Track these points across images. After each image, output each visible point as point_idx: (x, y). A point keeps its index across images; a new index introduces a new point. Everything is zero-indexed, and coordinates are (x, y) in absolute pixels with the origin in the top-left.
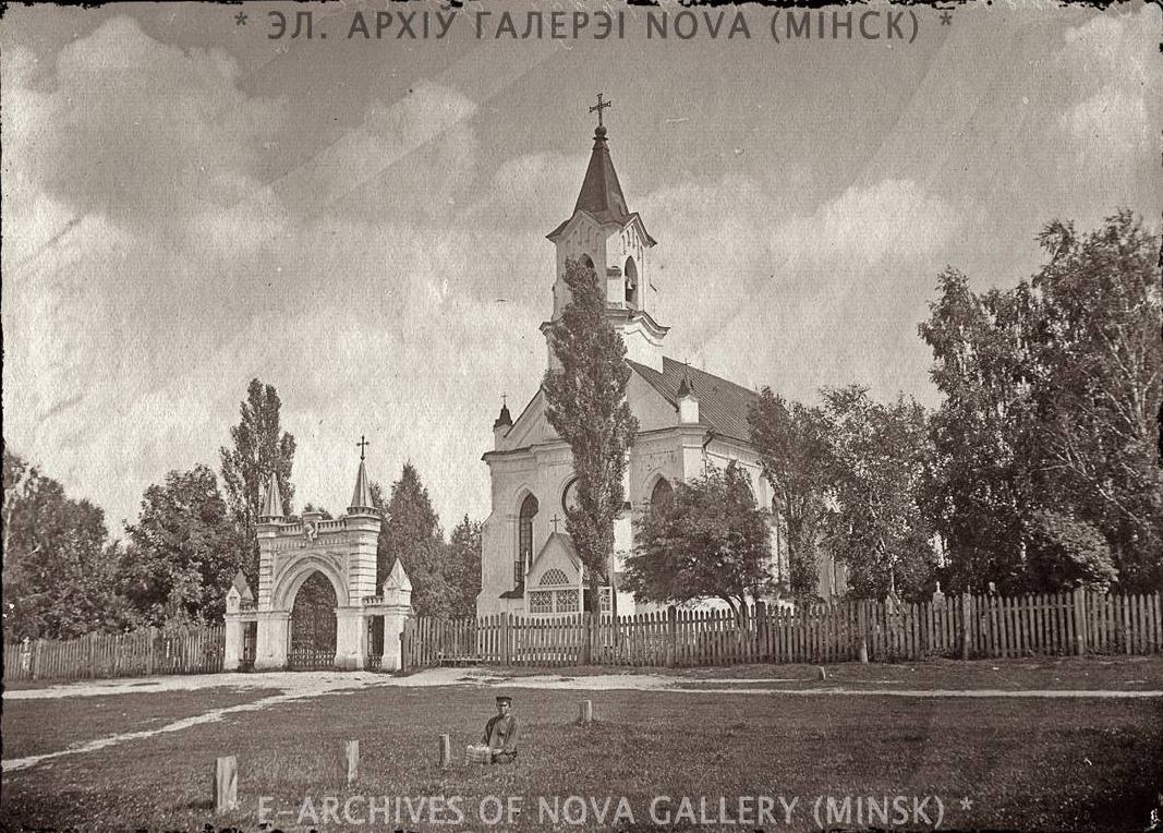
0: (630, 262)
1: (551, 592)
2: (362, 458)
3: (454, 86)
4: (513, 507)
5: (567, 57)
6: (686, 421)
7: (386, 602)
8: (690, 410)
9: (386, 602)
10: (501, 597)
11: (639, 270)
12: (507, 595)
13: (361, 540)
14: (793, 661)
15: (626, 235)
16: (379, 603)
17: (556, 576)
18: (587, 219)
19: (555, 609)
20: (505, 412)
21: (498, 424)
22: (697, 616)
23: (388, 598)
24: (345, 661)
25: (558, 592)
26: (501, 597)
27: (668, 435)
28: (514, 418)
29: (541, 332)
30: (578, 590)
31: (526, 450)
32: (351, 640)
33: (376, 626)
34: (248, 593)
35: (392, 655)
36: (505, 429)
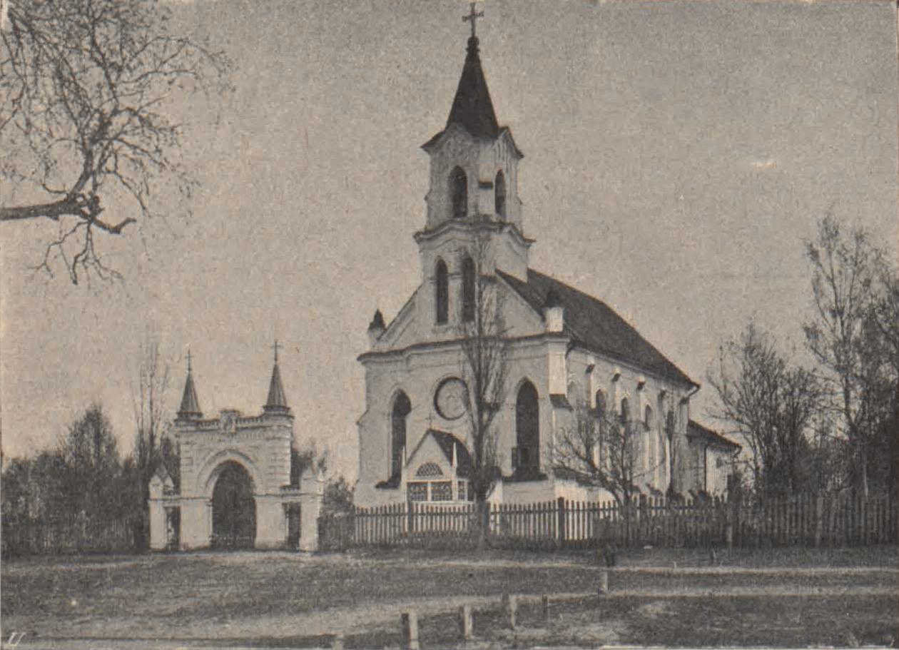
1: (426, 483)
4: (385, 405)
6: (551, 330)
9: (302, 491)
10: (377, 487)
12: (382, 486)
14: (735, 544)
20: (378, 318)
23: (304, 486)
26: (377, 487)
27: (527, 343)
28: (387, 322)
33: (293, 512)
35: (309, 538)
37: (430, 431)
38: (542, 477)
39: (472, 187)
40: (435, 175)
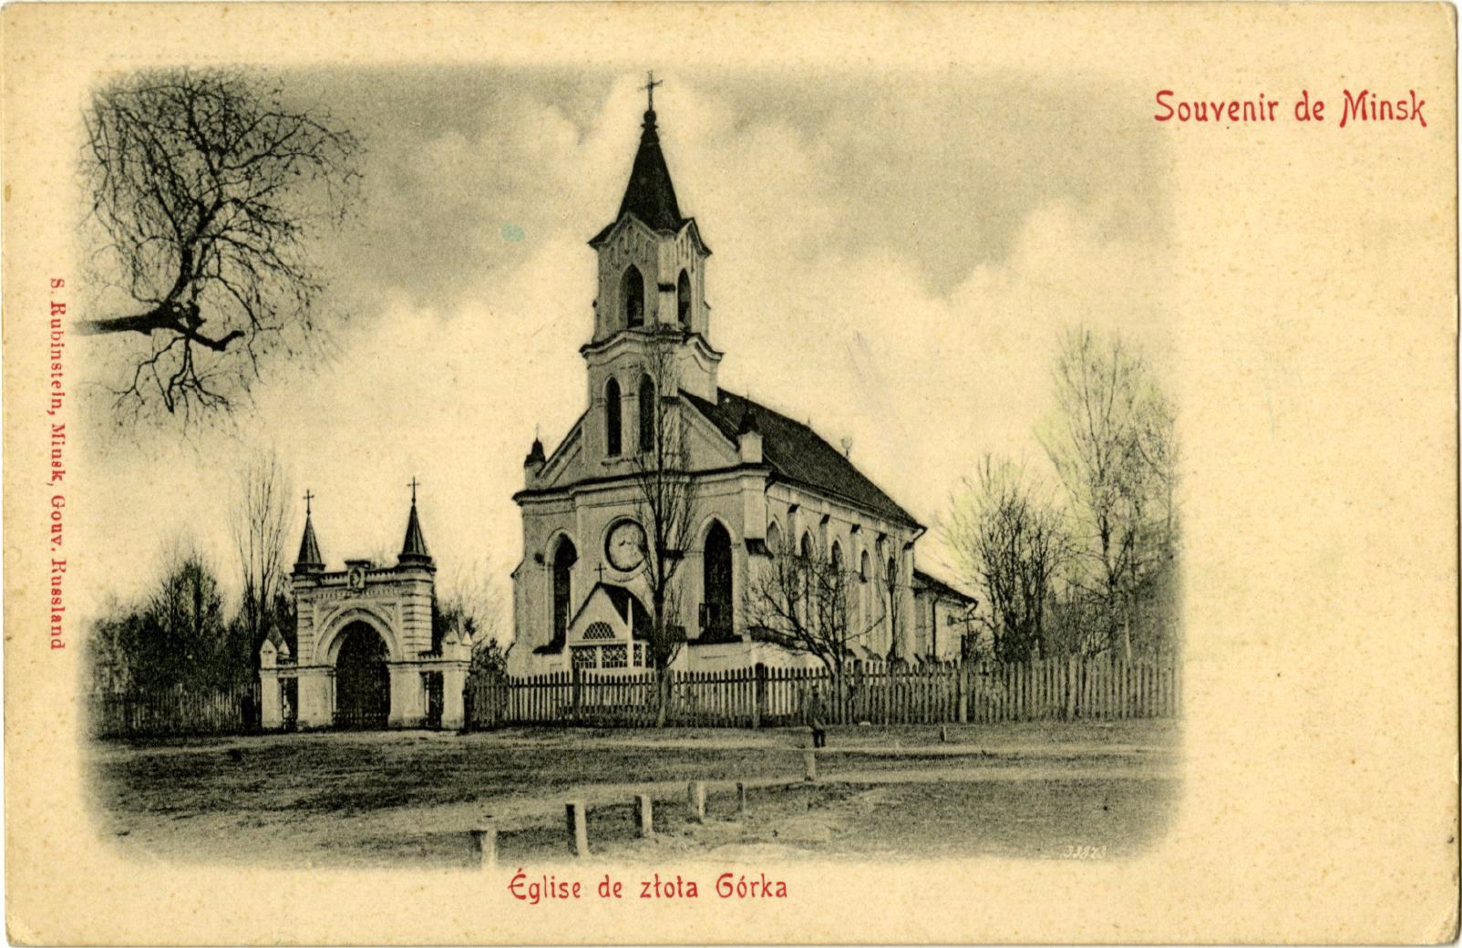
0: (684, 277)
1: (595, 647)
2: (309, 512)
3: (505, 76)
7: (445, 657)
9: (445, 657)
17: (602, 629)
19: (599, 663)
20: (538, 447)
21: (529, 461)
25: (603, 647)
28: (548, 454)
29: (580, 355)
32: (407, 698)
34: (285, 648)
36: (538, 465)
38: (739, 639)
39: (649, 289)
40: (603, 276)
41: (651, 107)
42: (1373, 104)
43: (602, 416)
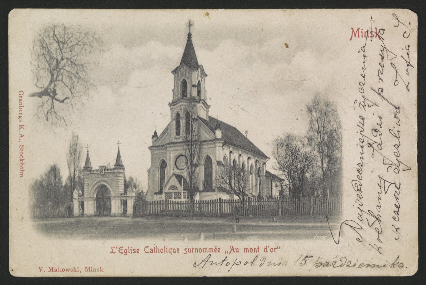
0: (199, 82)
5: (266, 31)
7: (128, 195)
8: (219, 134)
9: (128, 195)
11: (202, 85)
13: (119, 175)
15: (198, 73)
16: (125, 195)
18: (185, 68)
21: (153, 137)
22: (162, 202)
23: (129, 194)
24: (115, 214)
28: (159, 135)
30: (181, 192)
31: (163, 146)
34: (81, 192)
36: (155, 139)
37: (174, 174)
39: (189, 85)
41: (190, 32)
42: (362, 32)
43: (174, 122)
